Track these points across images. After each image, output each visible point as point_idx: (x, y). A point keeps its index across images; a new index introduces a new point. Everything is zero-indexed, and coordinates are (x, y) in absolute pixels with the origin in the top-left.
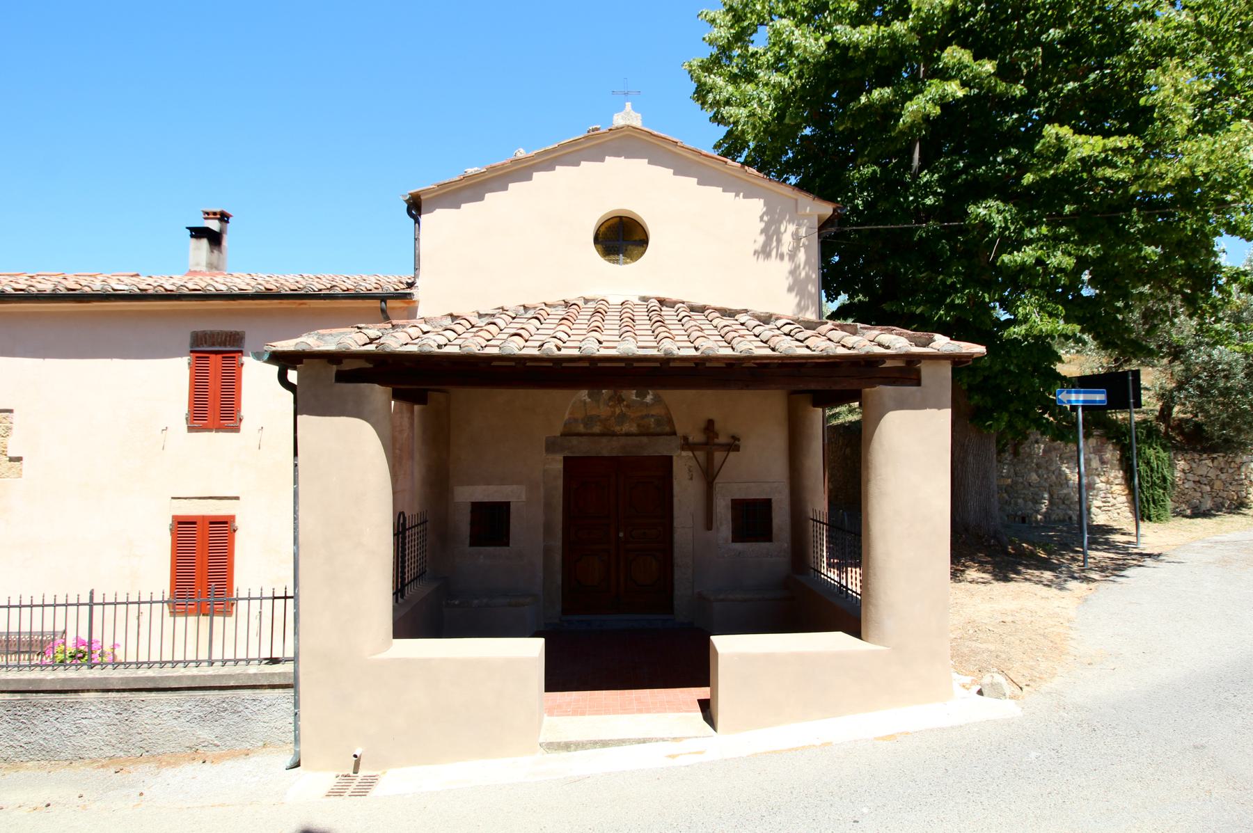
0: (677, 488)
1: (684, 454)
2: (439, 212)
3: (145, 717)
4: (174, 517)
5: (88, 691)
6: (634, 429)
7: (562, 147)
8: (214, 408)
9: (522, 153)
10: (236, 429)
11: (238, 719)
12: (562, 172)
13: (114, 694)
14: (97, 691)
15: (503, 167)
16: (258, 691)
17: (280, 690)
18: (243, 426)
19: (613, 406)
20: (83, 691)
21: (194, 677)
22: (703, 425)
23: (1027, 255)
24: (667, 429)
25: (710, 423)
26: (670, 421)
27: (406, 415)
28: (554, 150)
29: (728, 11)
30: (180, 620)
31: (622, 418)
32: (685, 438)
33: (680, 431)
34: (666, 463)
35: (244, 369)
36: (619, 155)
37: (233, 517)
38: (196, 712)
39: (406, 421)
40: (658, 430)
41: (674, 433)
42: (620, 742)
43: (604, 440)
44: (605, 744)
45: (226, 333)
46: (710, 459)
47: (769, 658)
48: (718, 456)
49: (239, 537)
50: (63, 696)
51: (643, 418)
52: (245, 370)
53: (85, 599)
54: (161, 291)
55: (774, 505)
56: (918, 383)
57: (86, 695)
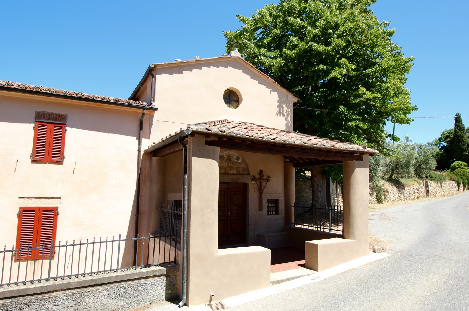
0: (250, 195)
1: (253, 182)
2: (164, 75)
3: (90, 299)
4: (20, 208)
5: (56, 291)
6: (235, 172)
7: (214, 59)
8: (48, 151)
9: (198, 58)
10: (61, 163)
11: (138, 294)
12: (212, 69)
13: (72, 291)
14: (62, 290)
15: (191, 62)
16: (147, 279)
17: (158, 278)
18: (65, 161)
19: (228, 163)
20: (53, 292)
21: (100, 279)
22: (259, 172)
23: (353, 123)
24: (246, 173)
25: (261, 171)
26: (247, 169)
27: (148, 161)
28: (211, 60)
29: (254, 20)
30: (23, 264)
31: (231, 168)
32: (254, 176)
33: (251, 174)
34: (245, 186)
35: (67, 133)
36: (233, 67)
37: (57, 208)
38: (117, 293)
39: (148, 164)
40: (243, 173)
41: (249, 174)
42: (293, 278)
43: (226, 176)
44: (289, 279)
45: (57, 114)
46: (261, 183)
47: (330, 245)
48: (264, 183)
49: (60, 218)
50: (40, 296)
51: (238, 168)
52: (67, 134)
53: (117, 238)
54: (23, 88)
55: (280, 201)
56: (362, 160)
57: (55, 293)
